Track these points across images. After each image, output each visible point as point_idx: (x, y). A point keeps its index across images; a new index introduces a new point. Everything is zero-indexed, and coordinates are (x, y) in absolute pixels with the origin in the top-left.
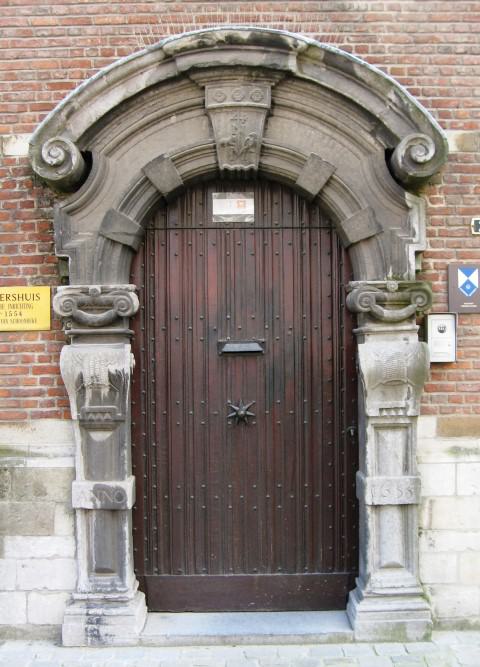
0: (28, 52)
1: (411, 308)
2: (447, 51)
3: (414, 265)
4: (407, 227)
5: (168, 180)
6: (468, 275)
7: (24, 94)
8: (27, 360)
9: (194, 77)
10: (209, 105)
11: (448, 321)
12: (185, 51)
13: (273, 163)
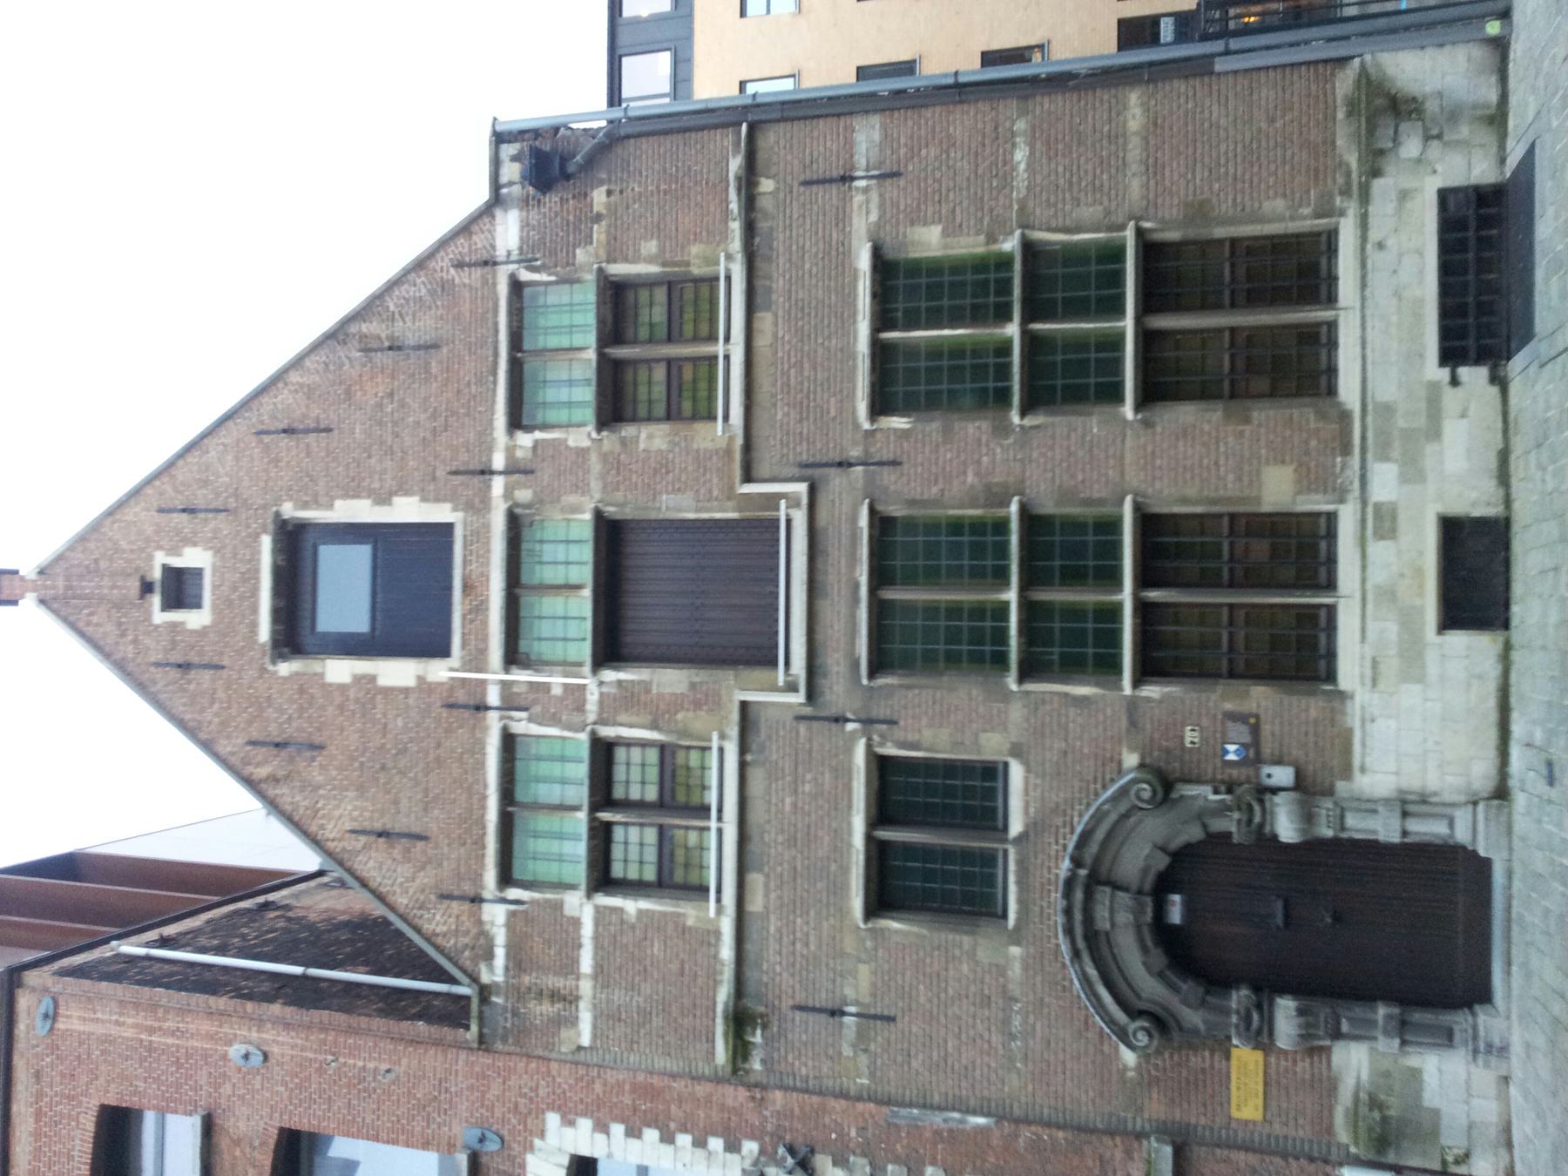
0: (1061, 1044)
4: (1194, 798)
5: (1159, 958)
7: (1091, 1050)
8: (1286, 1070)
13: (1148, 886)
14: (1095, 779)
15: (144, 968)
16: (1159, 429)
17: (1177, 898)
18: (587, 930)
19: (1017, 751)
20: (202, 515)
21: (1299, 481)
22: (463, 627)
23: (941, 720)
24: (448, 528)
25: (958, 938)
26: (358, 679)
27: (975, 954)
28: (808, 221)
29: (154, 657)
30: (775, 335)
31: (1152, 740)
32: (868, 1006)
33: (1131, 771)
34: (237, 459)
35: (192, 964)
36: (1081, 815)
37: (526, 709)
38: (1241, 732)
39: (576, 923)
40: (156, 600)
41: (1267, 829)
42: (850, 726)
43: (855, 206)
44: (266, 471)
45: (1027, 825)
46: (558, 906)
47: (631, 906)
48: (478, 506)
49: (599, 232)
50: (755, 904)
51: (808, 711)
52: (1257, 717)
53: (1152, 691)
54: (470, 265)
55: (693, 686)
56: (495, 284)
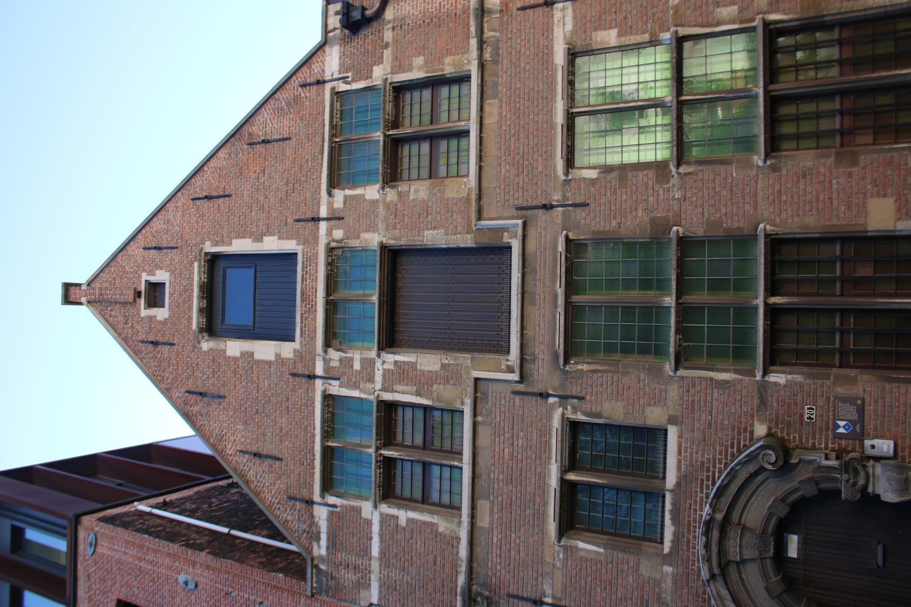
1: (859, 468)
2: (710, 424)
3: (833, 463)
6: (839, 427)
9: (723, 565)
10: (738, 559)
11: (868, 443)
12: (710, 569)
14: (732, 444)
15: (145, 520)
16: (784, 172)
17: (795, 538)
18: (376, 528)
19: (673, 420)
20: (165, 251)
21: (899, 210)
22: (302, 323)
23: (618, 395)
24: (293, 256)
25: (626, 556)
26: (243, 354)
27: (638, 570)
28: (523, 34)
29: (142, 336)
30: (500, 114)
31: (777, 416)
32: (560, 599)
33: (759, 440)
34: (183, 216)
35: (172, 520)
36: (720, 472)
37: (339, 379)
38: (851, 412)
39: (369, 523)
40: (142, 301)
41: (870, 490)
42: (551, 400)
43: (556, 21)
44: (197, 222)
45: (679, 478)
46: (359, 510)
47: (403, 516)
48: (311, 240)
49: (387, 53)
50: (484, 522)
51: (521, 387)
52: (863, 400)
53: (778, 378)
54: (310, 85)
55: (443, 366)
56: (324, 95)
